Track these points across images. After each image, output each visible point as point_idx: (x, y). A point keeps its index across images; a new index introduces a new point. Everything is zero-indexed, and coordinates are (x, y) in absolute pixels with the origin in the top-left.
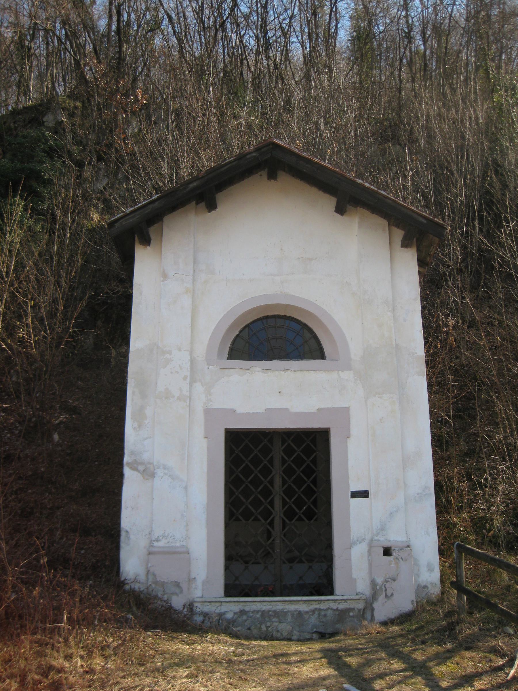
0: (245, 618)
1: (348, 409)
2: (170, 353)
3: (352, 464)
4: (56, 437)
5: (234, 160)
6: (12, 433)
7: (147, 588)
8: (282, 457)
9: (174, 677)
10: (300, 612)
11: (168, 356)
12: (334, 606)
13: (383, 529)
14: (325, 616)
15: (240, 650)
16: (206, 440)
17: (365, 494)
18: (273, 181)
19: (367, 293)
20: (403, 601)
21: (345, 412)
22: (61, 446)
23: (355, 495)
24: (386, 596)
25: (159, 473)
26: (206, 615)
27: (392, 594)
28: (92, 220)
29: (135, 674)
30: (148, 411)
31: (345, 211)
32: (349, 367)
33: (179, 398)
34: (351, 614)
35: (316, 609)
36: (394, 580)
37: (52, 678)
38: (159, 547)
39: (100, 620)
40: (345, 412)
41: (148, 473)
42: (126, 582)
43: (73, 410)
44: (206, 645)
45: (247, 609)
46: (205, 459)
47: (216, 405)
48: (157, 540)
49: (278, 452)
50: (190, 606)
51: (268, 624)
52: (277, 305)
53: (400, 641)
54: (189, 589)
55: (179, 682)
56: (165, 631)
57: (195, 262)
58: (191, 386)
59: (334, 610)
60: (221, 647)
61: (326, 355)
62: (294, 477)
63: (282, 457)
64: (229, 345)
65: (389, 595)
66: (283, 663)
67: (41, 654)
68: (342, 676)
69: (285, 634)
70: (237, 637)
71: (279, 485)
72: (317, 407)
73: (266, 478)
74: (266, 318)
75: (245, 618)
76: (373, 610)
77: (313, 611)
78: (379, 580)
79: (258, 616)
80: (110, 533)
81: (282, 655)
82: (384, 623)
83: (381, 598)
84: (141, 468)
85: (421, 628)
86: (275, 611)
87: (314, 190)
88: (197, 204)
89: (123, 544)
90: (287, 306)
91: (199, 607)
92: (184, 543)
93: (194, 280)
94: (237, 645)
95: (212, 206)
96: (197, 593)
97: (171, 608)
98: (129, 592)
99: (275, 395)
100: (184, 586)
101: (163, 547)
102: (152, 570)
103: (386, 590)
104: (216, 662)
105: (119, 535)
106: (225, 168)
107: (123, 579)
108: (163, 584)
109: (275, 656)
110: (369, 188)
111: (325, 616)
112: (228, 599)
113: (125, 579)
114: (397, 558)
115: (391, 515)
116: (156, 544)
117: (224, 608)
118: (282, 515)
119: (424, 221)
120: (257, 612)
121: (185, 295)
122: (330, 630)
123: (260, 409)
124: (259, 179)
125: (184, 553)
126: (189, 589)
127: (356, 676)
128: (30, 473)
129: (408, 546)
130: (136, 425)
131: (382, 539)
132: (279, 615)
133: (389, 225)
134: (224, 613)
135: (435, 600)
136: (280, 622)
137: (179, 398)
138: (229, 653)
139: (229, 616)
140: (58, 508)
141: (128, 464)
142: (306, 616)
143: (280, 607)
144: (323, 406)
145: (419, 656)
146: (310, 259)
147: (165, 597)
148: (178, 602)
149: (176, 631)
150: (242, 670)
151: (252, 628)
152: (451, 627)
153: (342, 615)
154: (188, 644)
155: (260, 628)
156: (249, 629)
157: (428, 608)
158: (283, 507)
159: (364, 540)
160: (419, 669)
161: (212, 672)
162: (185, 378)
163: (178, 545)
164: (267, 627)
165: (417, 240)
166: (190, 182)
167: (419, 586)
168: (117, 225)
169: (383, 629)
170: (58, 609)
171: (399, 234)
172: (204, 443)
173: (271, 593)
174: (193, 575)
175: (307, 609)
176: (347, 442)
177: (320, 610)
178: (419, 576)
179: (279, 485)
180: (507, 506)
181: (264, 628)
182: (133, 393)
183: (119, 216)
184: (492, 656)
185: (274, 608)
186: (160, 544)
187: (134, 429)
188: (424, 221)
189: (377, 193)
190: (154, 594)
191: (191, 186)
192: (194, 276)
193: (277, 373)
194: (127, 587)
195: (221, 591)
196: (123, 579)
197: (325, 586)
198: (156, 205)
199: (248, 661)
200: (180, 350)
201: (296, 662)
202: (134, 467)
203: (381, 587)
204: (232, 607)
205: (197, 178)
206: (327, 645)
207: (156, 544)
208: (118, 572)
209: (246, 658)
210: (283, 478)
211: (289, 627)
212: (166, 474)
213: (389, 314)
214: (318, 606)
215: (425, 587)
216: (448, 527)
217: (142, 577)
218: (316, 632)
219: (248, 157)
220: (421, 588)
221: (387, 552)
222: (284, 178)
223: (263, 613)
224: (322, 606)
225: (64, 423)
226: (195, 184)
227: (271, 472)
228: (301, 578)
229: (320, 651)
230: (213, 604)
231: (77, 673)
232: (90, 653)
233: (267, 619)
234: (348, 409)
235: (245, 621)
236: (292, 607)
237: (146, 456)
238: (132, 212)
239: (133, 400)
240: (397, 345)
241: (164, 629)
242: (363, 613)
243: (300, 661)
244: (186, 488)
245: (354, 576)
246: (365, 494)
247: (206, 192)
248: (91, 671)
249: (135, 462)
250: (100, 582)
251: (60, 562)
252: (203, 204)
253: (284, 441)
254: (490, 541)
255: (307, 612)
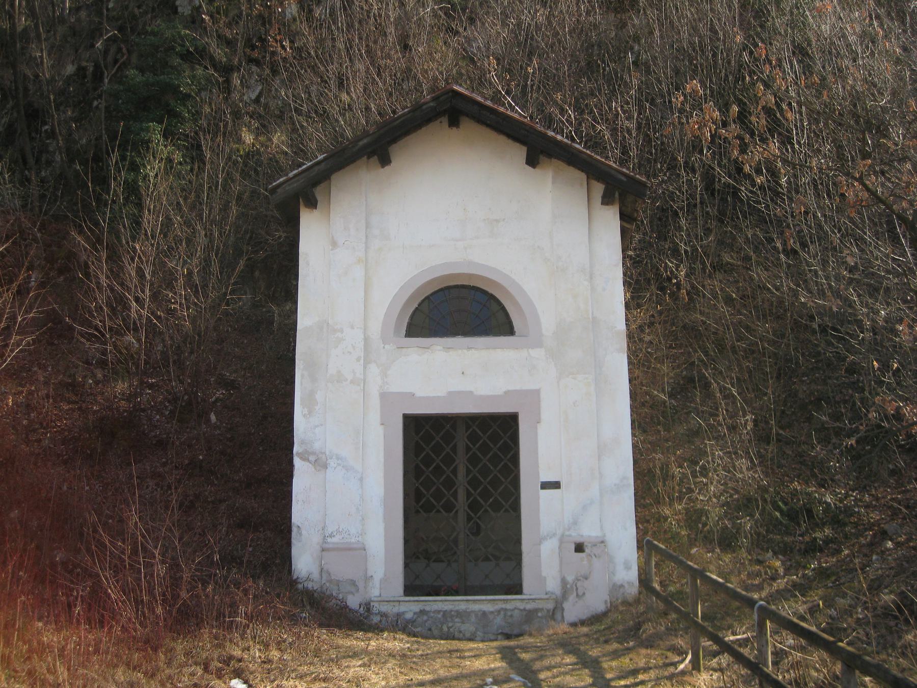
0: (425, 618)
1: (537, 392)
2: (342, 331)
3: (544, 451)
4: (213, 418)
5: (409, 112)
6: (162, 415)
7: (321, 587)
8: (467, 445)
9: (348, 667)
10: (484, 614)
11: (339, 334)
12: (521, 606)
13: (575, 523)
14: (511, 616)
15: (416, 646)
16: (382, 427)
17: (556, 485)
18: (454, 129)
19: (562, 256)
20: (595, 600)
21: (534, 396)
22: (220, 429)
23: (546, 486)
24: (577, 595)
25: (332, 463)
26: (384, 615)
27: (584, 594)
28: (244, 143)
29: (310, 664)
30: (319, 396)
31: (538, 163)
32: (539, 344)
33: (352, 382)
34: (540, 614)
35: (502, 609)
36: (586, 579)
37: (234, 666)
38: (333, 543)
39: (273, 618)
40: (534, 396)
41: (320, 463)
42: (299, 580)
43: (230, 385)
44: (381, 641)
45: (427, 608)
46: (382, 448)
47: (394, 388)
48: (331, 536)
49: (461, 438)
50: (368, 606)
51: (450, 625)
52: (459, 275)
53: (582, 640)
54: (365, 587)
55: (352, 670)
56: (340, 629)
57: (368, 226)
58: (365, 367)
59: (521, 610)
60: (397, 643)
61: (515, 329)
62: (479, 466)
63: (467, 445)
64: (407, 320)
65: (580, 593)
66: (457, 657)
67: (220, 646)
68: (512, 668)
69: (468, 635)
70: (415, 636)
71: (462, 473)
72: (504, 390)
73: (474, 453)
74: (449, 288)
75: (425, 618)
76: (563, 610)
77: (499, 612)
78: (570, 579)
79: (440, 616)
80: (281, 528)
81: (457, 651)
82: (574, 625)
83: (572, 598)
84: (312, 458)
85: (609, 628)
86: (457, 611)
87: (502, 139)
88: (369, 158)
89: (294, 541)
90: (471, 276)
91: (376, 608)
92: (360, 539)
93: (367, 248)
94: (413, 643)
95: (385, 161)
96: (374, 592)
97: (346, 607)
98: (302, 592)
99: (458, 376)
100: (361, 585)
101: (337, 543)
102: (325, 568)
103: (577, 589)
104: (390, 655)
105: (290, 531)
106: (398, 122)
107: (295, 577)
108: (338, 583)
109: (450, 652)
110: (561, 142)
111: (511, 616)
112: (408, 598)
113: (298, 578)
114: (590, 555)
115: (585, 508)
116: (329, 540)
117: (402, 608)
118: (466, 508)
119: (623, 178)
120: (439, 612)
121: (358, 261)
122: (516, 632)
123: (442, 392)
124: (440, 127)
125: (360, 549)
126: (365, 587)
127: (527, 672)
128: (187, 462)
129: (602, 542)
130: (306, 411)
131: (573, 534)
132: (463, 616)
133: (588, 178)
134: (403, 613)
135: (630, 600)
136: (463, 623)
137: (352, 382)
138: (404, 649)
139: (409, 616)
140: (221, 501)
141: (298, 454)
142: (491, 617)
143: (462, 607)
144: (511, 388)
145: (594, 652)
146: (497, 221)
147: (341, 597)
148: (353, 602)
149: (351, 630)
150: (414, 663)
151: (433, 629)
152: (638, 626)
153: (530, 616)
154: (363, 641)
155: (441, 629)
156: (430, 630)
157: (621, 608)
158: (468, 500)
159: (554, 535)
160: (593, 665)
161: (385, 663)
162: (358, 359)
163: (353, 540)
164: (449, 628)
165: (620, 195)
166: (357, 139)
167: (614, 585)
168: (279, 190)
169: (572, 630)
170: (233, 606)
171: (599, 189)
172: (380, 430)
173: (457, 593)
174: (369, 573)
175: (492, 609)
176: (536, 428)
177: (506, 610)
178: (614, 575)
179: (462, 473)
180: (731, 496)
181: (445, 628)
182: (302, 376)
183: (281, 180)
184: (669, 654)
185: (457, 608)
186: (334, 540)
187: (304, 416)
188: (623, 178)
189: (571, 146)
190: (328, 593)
191: (361, 143)
192: (366, 243)
193: (460, 351)
194: (300, 586)
195: (401, 590)
196: (295, 577)
197: (517, 589)
198: (323, 166)
199: (422, 655)
200: (352, 327)
201: (469, 657)
202: (304, 458)
203: (572, 587)
204: (411, 607)
205: (366, 134)
206: (506, 643)
207: (329, 540)
208: (290, 571)
209: (420, 653)
210: (467, 467)
211: (472, 629)
212: (339, 464)
213: (586, 283)
214: (504, 606)
215: (622, 586)
216: (658, 521)
217: (316, 575)
218: (502, 633)
219: (424, 107)
220: (616, 588)
221: (579, 548)
222: (468, 126)
223: (445, 613)
224: (508, 606)
225: (221, 400)
226: (365, 141)
227: (454, 461)
228: (487, 576)
229: (496, 648)
230: (392, 604)
231: (255, 662)
232: (267, 646)
233: (449, 619)
234: (537, 392)
235: (426, 621)
236: (476, 607)
237: (317, 446)
238: (295, 176)
239: (302, 384)
240: (594, 318)
241: (340, 627)
242: (553, 613)
243: (474, 656)
244: (361, 479)
245: (544, 574)
246: (556, 485)
247: (378, 146)
248: (270, 661)
249: (306, 451)
250: (271, 581)
251: (230, 560)
252: (376, 157)
253: (468, 427)
254: (705, 537)
255: (492, 612)
